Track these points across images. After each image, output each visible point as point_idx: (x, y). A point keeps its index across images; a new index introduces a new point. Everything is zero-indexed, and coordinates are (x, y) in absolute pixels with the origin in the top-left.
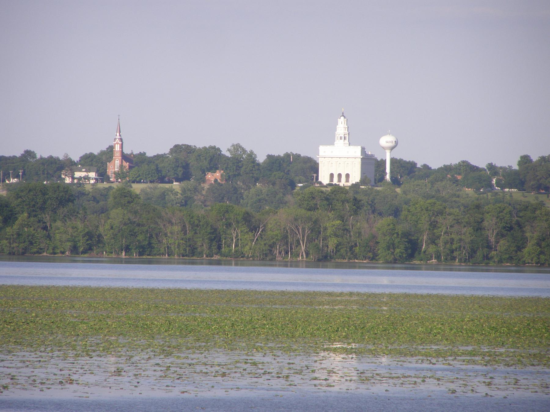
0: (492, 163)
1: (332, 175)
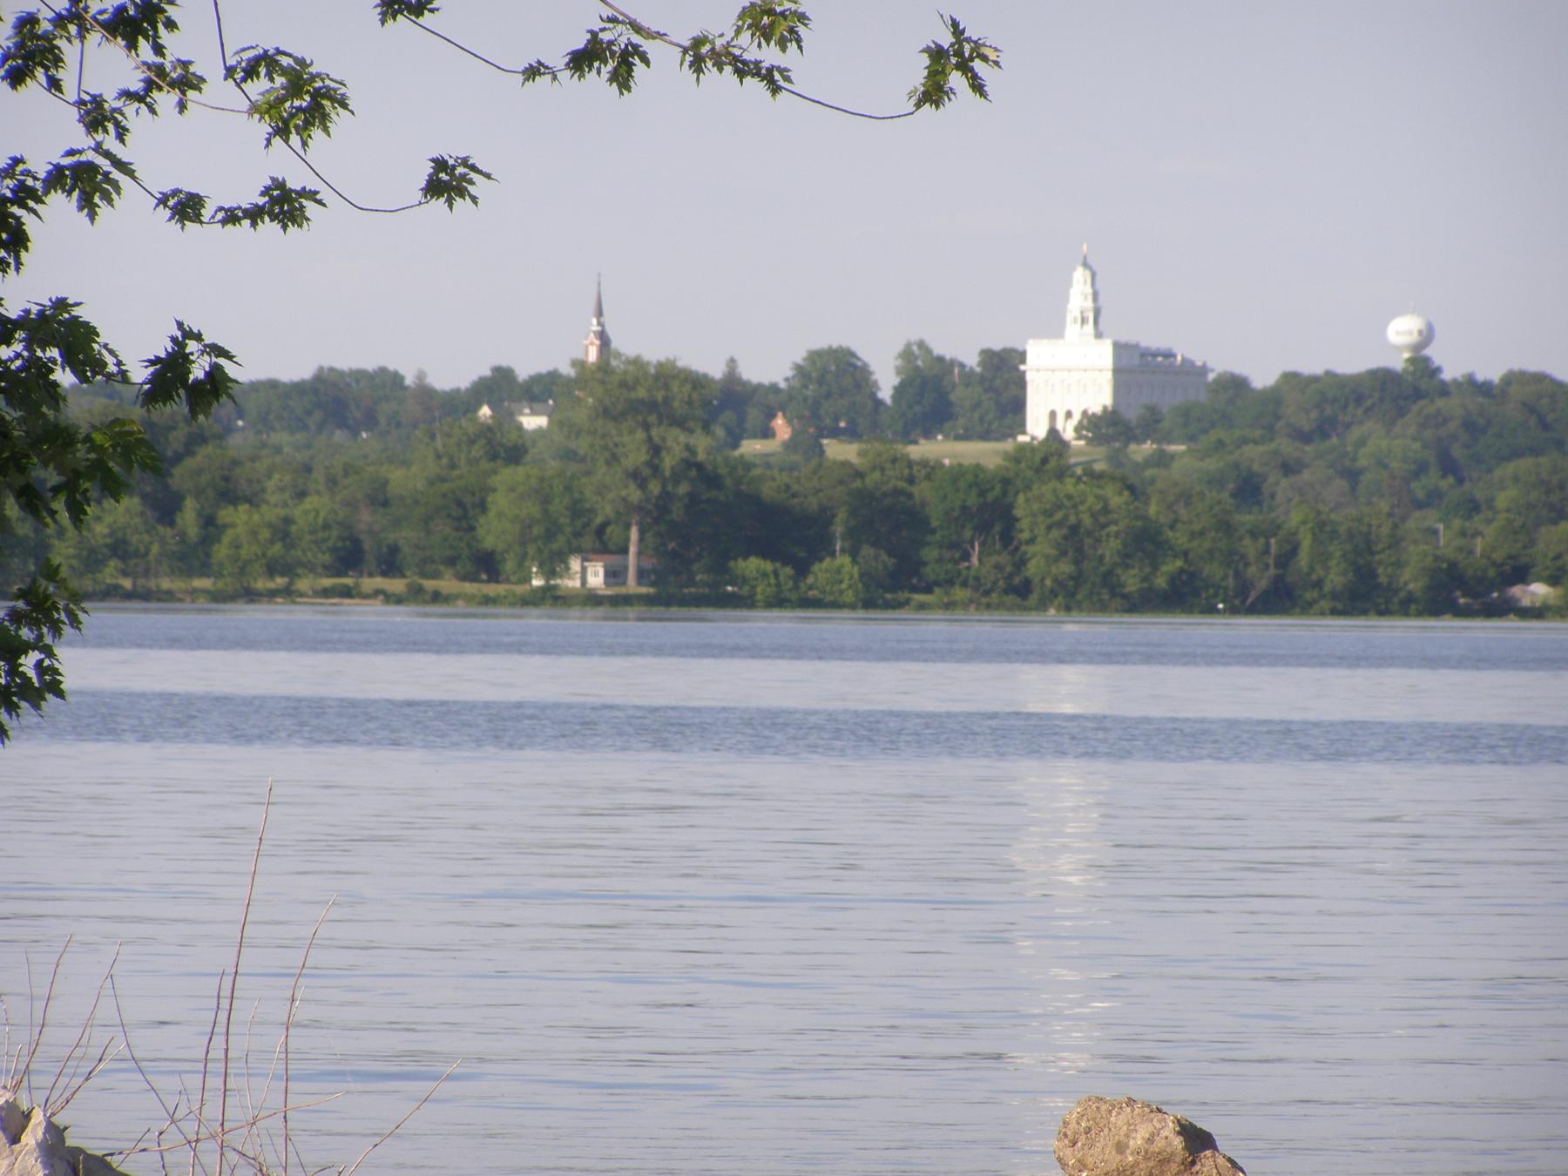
1: (1053, 415)
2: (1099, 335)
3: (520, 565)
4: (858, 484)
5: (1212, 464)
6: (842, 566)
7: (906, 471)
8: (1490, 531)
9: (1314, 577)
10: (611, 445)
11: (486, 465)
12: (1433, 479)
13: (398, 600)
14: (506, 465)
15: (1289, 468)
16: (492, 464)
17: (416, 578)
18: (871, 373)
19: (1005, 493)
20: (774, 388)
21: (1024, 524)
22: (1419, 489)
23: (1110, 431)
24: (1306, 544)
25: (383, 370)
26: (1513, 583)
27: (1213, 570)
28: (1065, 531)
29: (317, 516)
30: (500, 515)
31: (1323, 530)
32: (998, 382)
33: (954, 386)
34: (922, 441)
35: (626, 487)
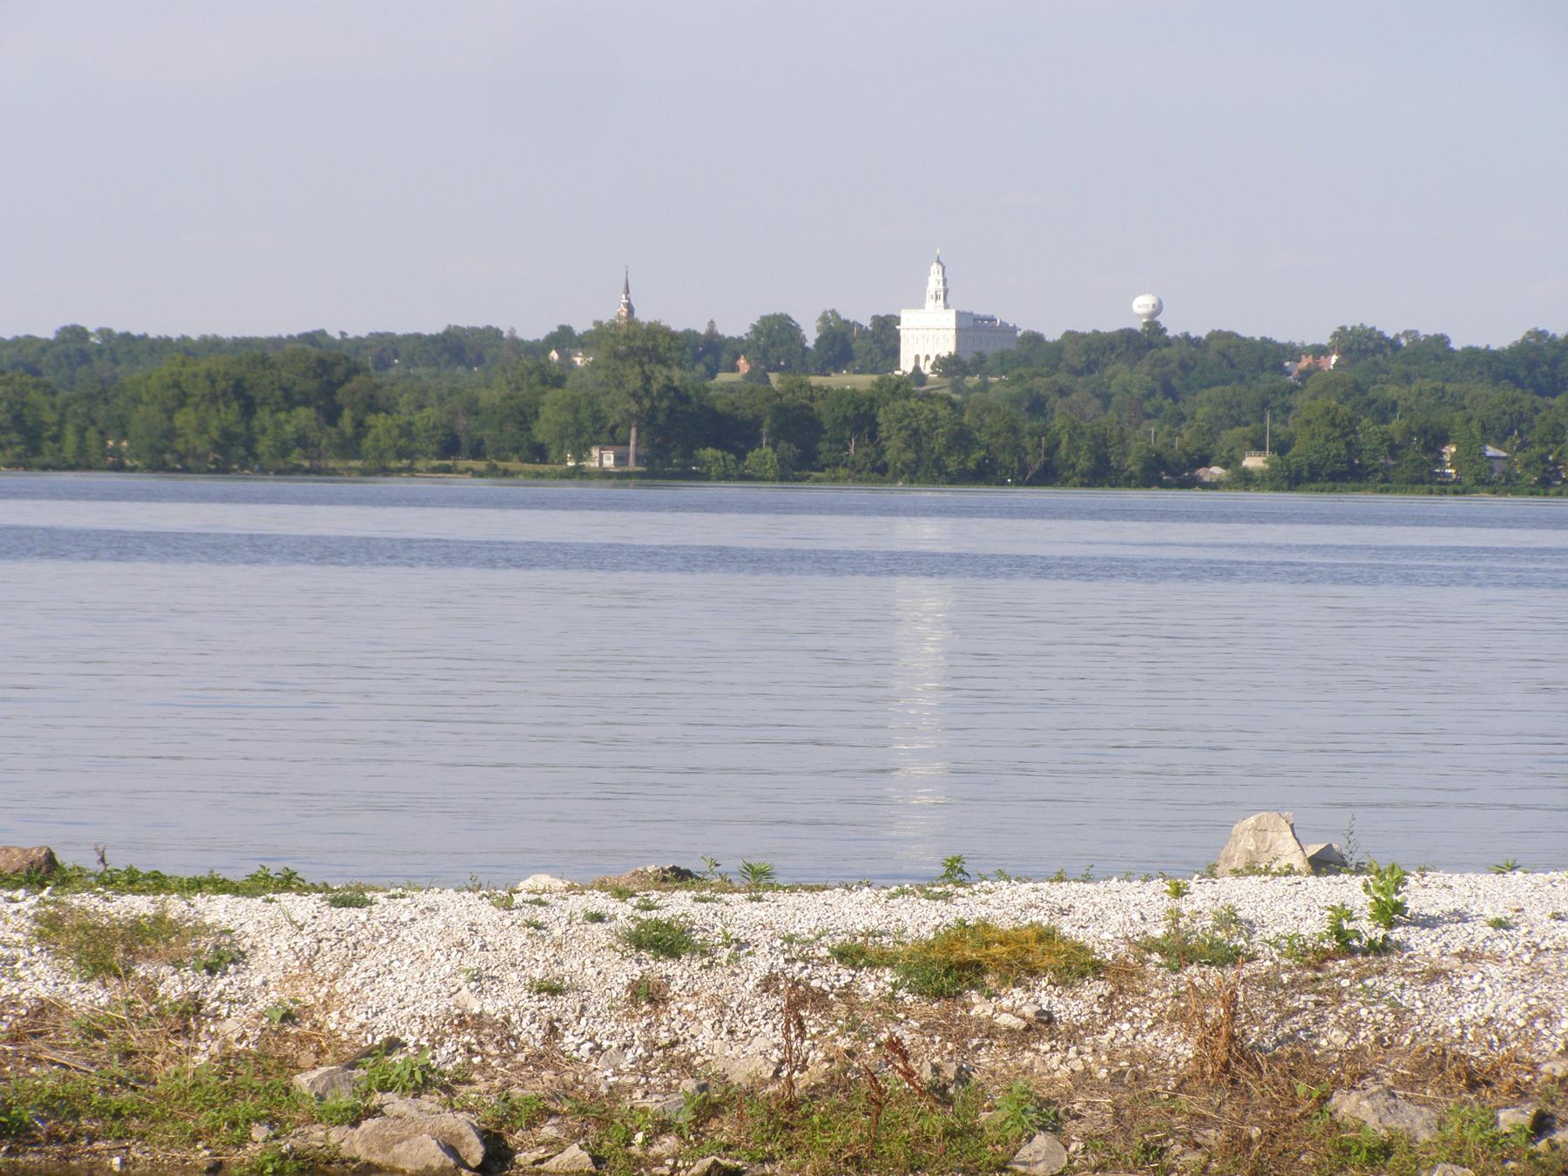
1: (917, 358)
2: (947, 307)
4: (778, 401)
8: (1187, 435)
9: (1070, 462)
10: (619, 376)
11: (539, 388)
12: (1158, 399)
13: (481, 475)
14: (552, 388)
15: (1063, 392)
16: (543, 388)
17: (494, 461)
18: (801, 330)
20: (740, 340)
21: (883, 427)
22: (1148, 406)
23: (953, 368)
24: (1065, 439)
25: (489, 328)
26: (1200, 467)
27: (1005, 458)
28: (909, 432)
29: (429, 420)
30: (547, 420)
31: (1075, 431)
32: (883, 337)
33: (855, 339)
34: (833, 374)
35: (629, 402)
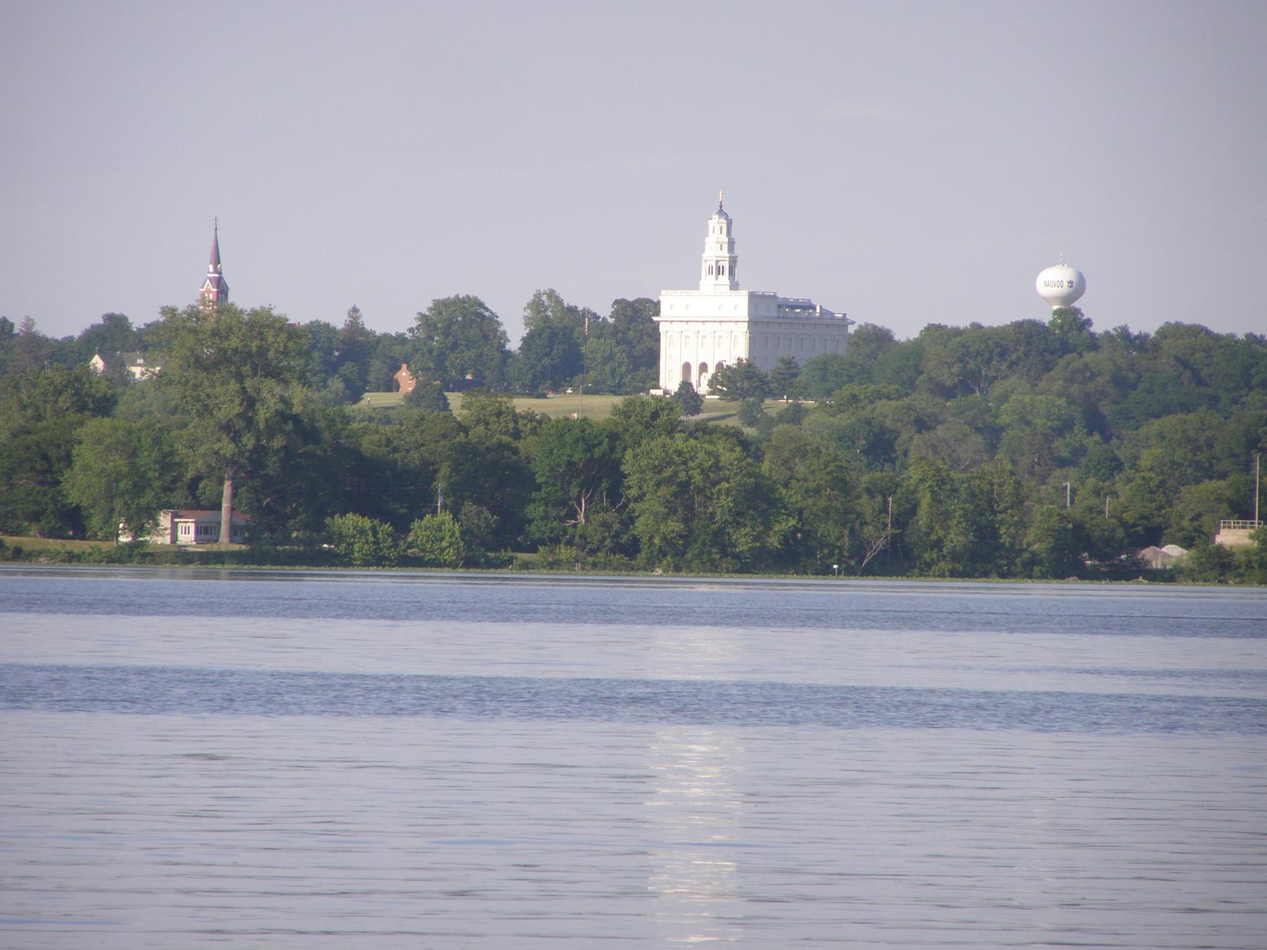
0: (1264, 336)
1: (687, 367)
2: (734, 286)
3: (107, 521)
4: (461, 437)
5: (844, 420)
6: (443, 523)
7: (511, 425)
9: (933, 537)
11: (73, 417)
12: (1079, 435)
19: (612, 450)
20: (400, 339)
21: (633, 480)
22: (1061, 447)
24: (925, 501)
26: (1145, 545)
27: (828, 530)
30: (86, 468)
33: (586, 339)
34: (550, 395)
35: (219, 440)
